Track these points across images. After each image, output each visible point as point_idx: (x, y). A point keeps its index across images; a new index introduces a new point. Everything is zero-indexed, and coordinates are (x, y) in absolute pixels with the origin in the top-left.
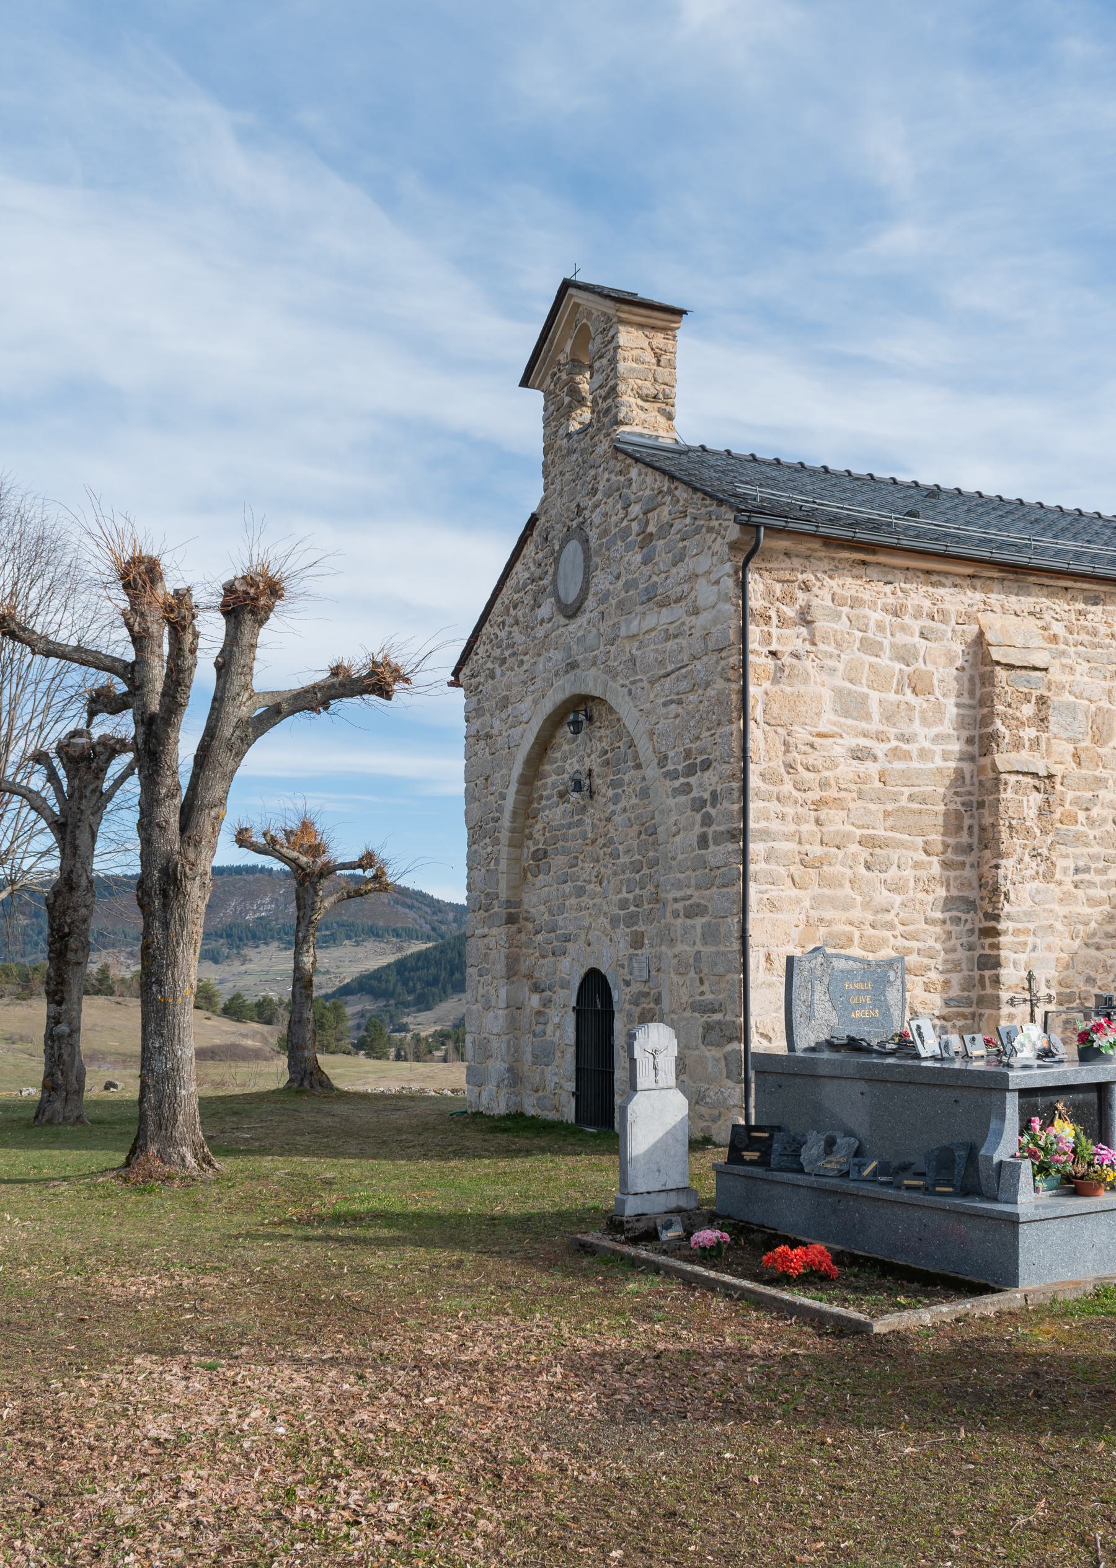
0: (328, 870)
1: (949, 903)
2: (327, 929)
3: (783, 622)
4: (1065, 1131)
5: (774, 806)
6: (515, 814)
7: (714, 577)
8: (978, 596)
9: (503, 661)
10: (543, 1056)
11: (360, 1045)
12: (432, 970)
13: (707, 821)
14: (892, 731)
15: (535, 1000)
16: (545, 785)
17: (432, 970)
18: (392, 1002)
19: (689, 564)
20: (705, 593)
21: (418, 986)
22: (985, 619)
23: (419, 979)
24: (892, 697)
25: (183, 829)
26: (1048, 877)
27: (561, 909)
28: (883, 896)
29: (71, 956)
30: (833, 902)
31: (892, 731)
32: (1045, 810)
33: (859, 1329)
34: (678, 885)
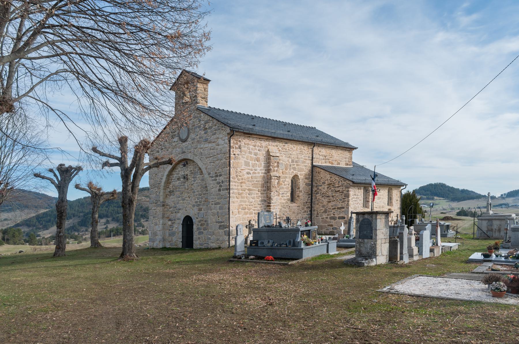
0: (103, 194)
1: (262, 201)
2: (11, 206)
3: (236, 148)
4: (305, 237)
5: (234, 183)
6: (165, 183)
7: (223, 139)
8: (268, 143)
9: (162, 149)
10: (172, 234)
11: (26, 241)
12: (49, 218)
13: (221, 186)
14: (253, 169)
15: (170, 223)
16: (173, 177)
17: (49, 218)
18: (35, 228)
19: (217, 136)
20: (220, 141)
21: (44, 223)
22: (269, 147)
23: (44, 221)
24: (254, 162)
25: (132, 191)
26: (278, 195)
27: (178, 203)
28: (251, 200)
29: (63, 217)
30: (243, 201)
31: (253, 169)
32: (278, 183)
33: (287, 264)
34: (213, 199)
